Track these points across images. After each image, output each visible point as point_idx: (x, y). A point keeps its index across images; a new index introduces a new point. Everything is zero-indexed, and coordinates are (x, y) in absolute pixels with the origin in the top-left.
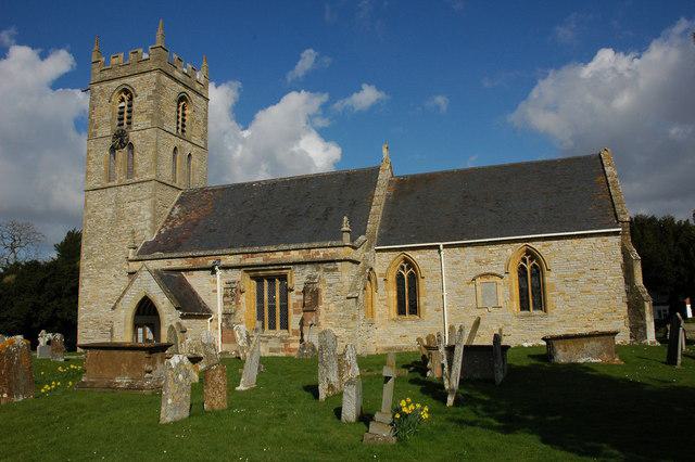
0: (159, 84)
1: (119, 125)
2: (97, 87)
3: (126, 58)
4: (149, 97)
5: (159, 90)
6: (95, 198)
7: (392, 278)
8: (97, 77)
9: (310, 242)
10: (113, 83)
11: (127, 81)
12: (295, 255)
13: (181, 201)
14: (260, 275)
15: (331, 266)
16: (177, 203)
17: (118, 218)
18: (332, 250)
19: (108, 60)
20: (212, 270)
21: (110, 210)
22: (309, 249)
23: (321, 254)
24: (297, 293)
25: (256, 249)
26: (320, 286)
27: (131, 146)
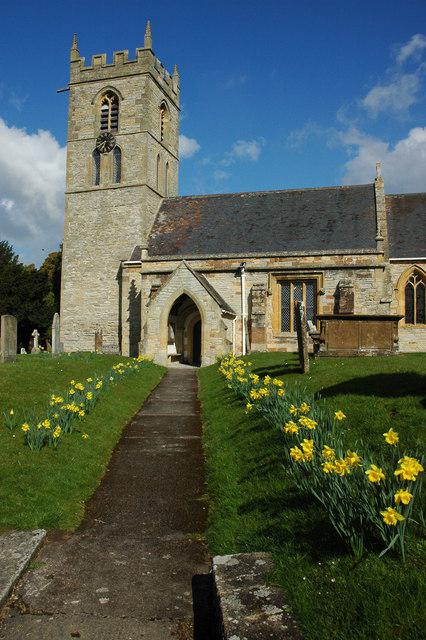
0: (146, 87)
1: (102, 128)
2: (77, 88)
3: (110, 59)
4: (138, 101)
5: (145, 98)
6: (76, 202)
7: (402, 288)
8: (77, 78)
9: (319, 249)
10: (96, 85)
11: (112, 83)
12: (326, 261)
13: (164, 208)
14: (285, 279)
15: (365, 272)
16: (161, 210)
17: (104, 222)
18: (365, 257)
19: (88, 62)
20: (238, 272)
21: (95, 214)
22: (343, 255)
23: (354, 260)
24: (328, 297)
25: (285, 253)
26: (354, 290)
27: (118, 150)
